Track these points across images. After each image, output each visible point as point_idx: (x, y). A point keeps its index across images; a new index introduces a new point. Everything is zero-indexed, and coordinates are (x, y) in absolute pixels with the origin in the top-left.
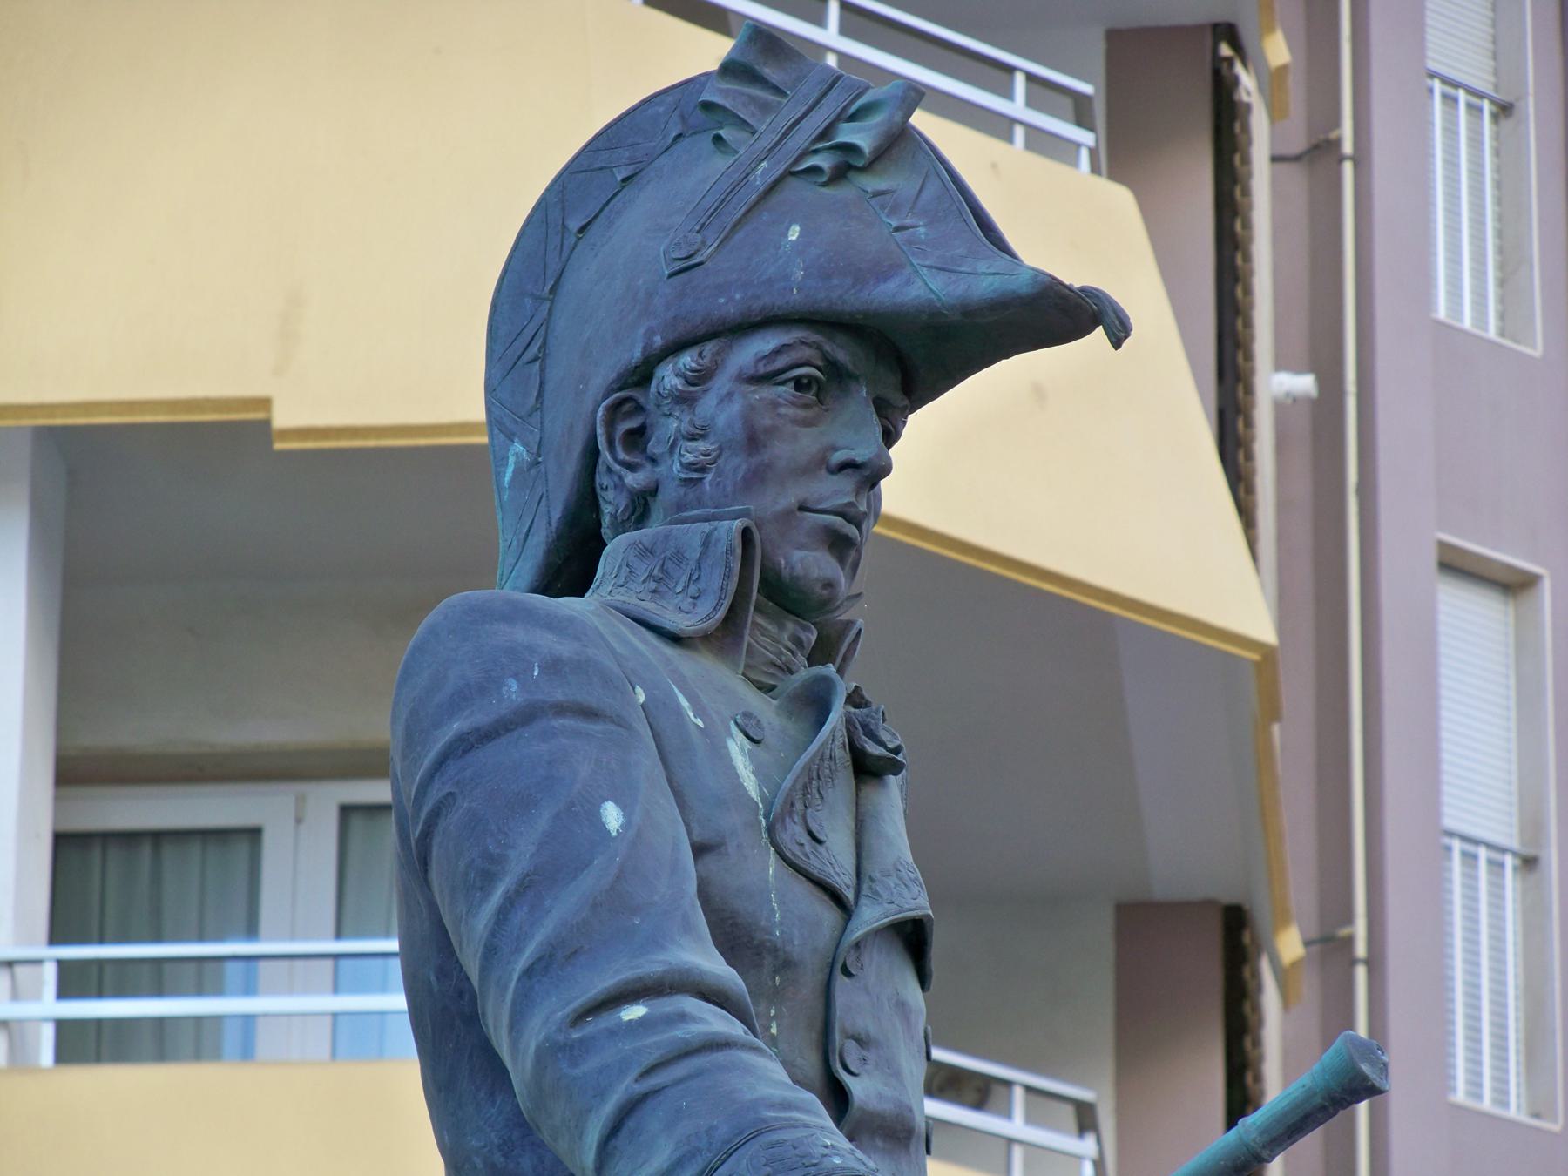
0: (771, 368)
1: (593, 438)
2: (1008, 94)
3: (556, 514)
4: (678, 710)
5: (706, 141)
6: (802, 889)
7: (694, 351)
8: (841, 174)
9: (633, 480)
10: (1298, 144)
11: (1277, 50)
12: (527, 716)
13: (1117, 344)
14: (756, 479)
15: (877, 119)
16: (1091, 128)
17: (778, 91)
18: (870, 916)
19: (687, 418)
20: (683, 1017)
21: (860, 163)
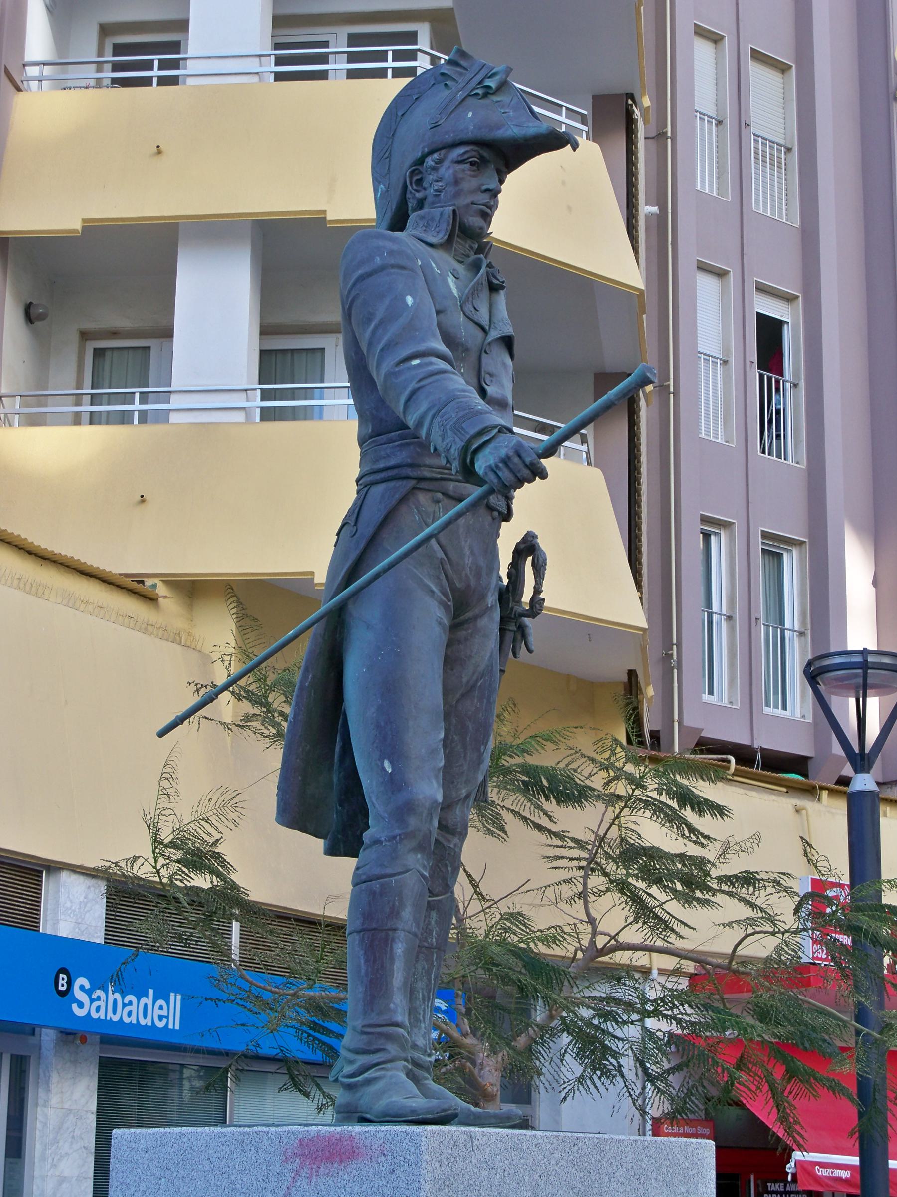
0: (462, 158)
1: (405, 182)
2: (561, 115)
3: (394, 207)
4: (432, 268)
5: (442, 85)
6: (471, 325)
7: (438, 153)
8: (485, 95)
9: (418, 195)
10: (654, 134)
11: (646, 102)
12: (382, 268)
13: (574, 150)
14: (457, 194)
15: (497, 78)
16: (587, 125)
17: (465, 69)
18: (494, 334)
19: (435, 175)
20: (431, 363)
21: (492, 92)
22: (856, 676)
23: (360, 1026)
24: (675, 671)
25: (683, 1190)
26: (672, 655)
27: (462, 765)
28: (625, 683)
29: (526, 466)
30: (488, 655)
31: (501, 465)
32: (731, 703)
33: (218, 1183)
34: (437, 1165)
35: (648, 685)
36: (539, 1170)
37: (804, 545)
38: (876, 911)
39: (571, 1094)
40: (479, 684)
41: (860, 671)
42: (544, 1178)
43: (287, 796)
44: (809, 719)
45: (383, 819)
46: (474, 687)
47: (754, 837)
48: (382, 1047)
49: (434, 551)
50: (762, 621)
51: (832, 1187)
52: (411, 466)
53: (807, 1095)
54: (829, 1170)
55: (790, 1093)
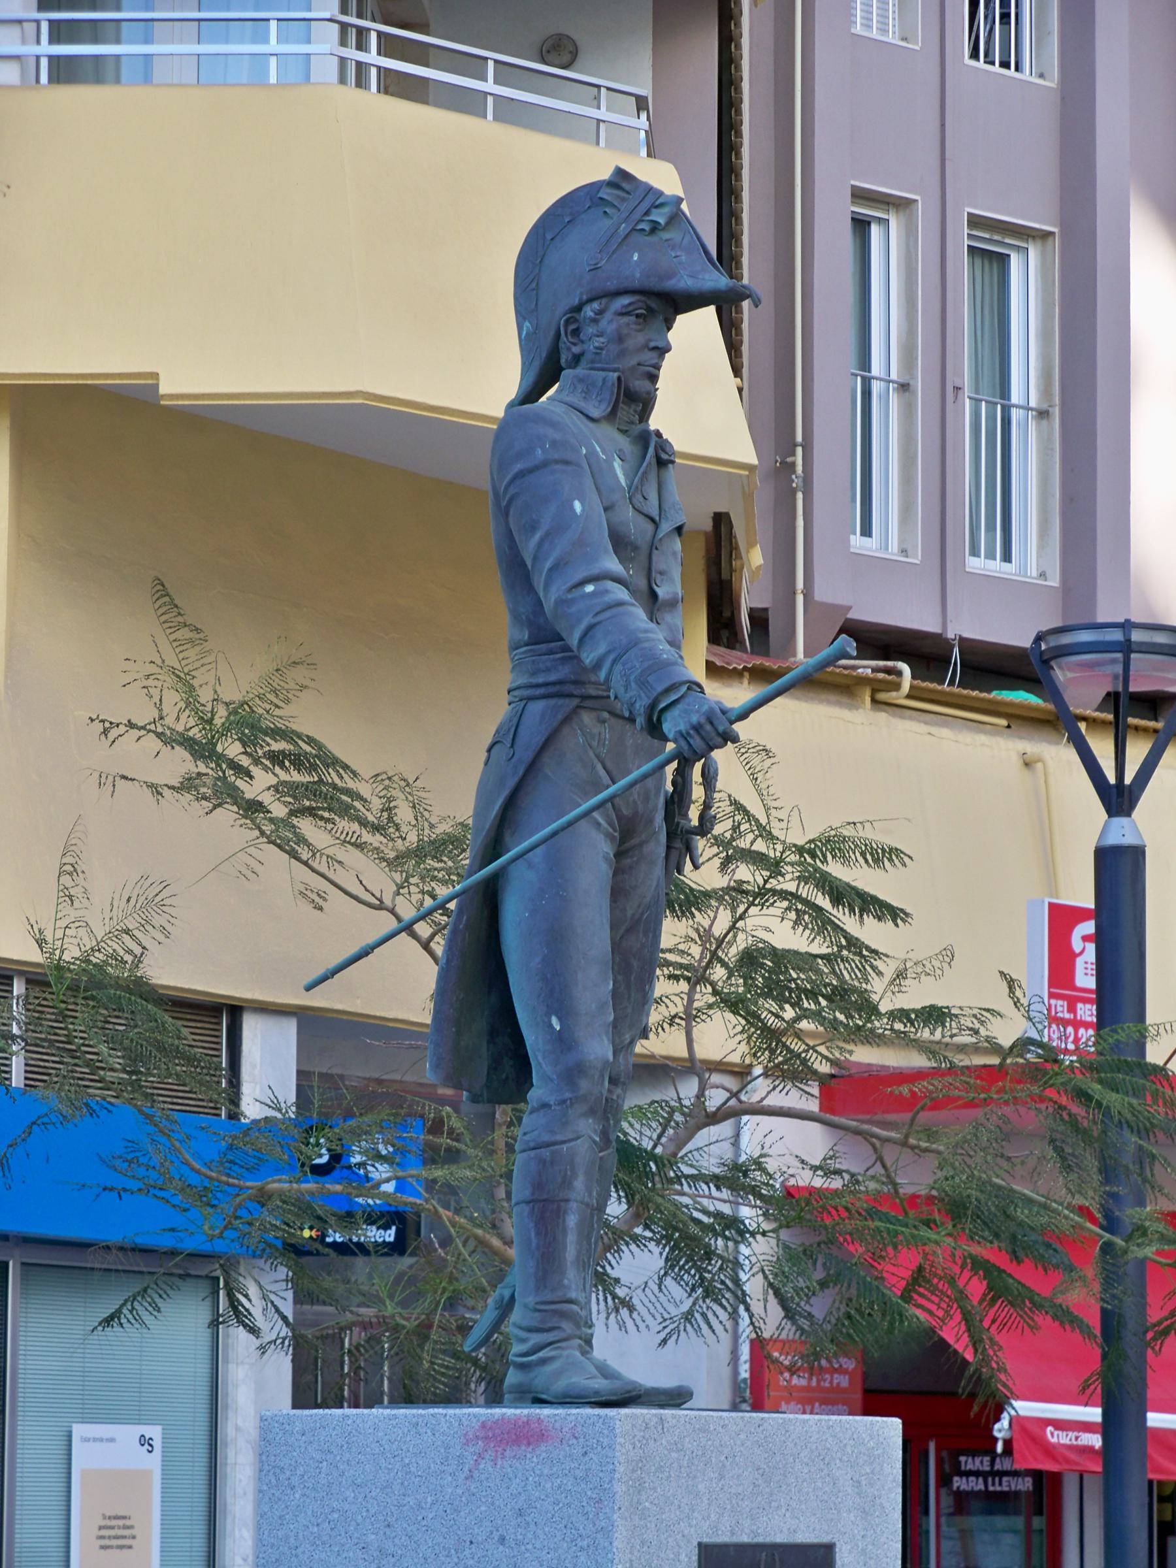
3: (544, 355)
6: (641, 519)
7: (598, 302)
9: (576, 350)
12: (545, 464)
14: (622, 354)
20: (607, 591)
22: (1114, 661)
23: (533, 1303)
24: (800, 496)
25: (868, 1471)
26: (793, 464)
27: (626, 1007)
28: (706, 533)
29: (719, 734)
30: (655, 884)
31: (692, 732)
32: (904, 552)
33: (390, 1466)
34: (631, 1447)
35: (751, 545)
36: (726, 1451)
37: (1051, 238)
38: (1119, 1072)
39: (675, 1337)
40: (645, 917)
41: (1119, 655)
42: (730, 1459)
43: (441, 1050)
44: (1054, 581)
45: (552, 1080)
46: (639, 921)
47: (944, 953)
48: (557, 1325)
49: (600, 778)
50: (967, 391)
51: (1077, 1464)
52: (575, 683)
53: (1020, 1325)
54: (1072, 1435)
55: (993, 1322)
